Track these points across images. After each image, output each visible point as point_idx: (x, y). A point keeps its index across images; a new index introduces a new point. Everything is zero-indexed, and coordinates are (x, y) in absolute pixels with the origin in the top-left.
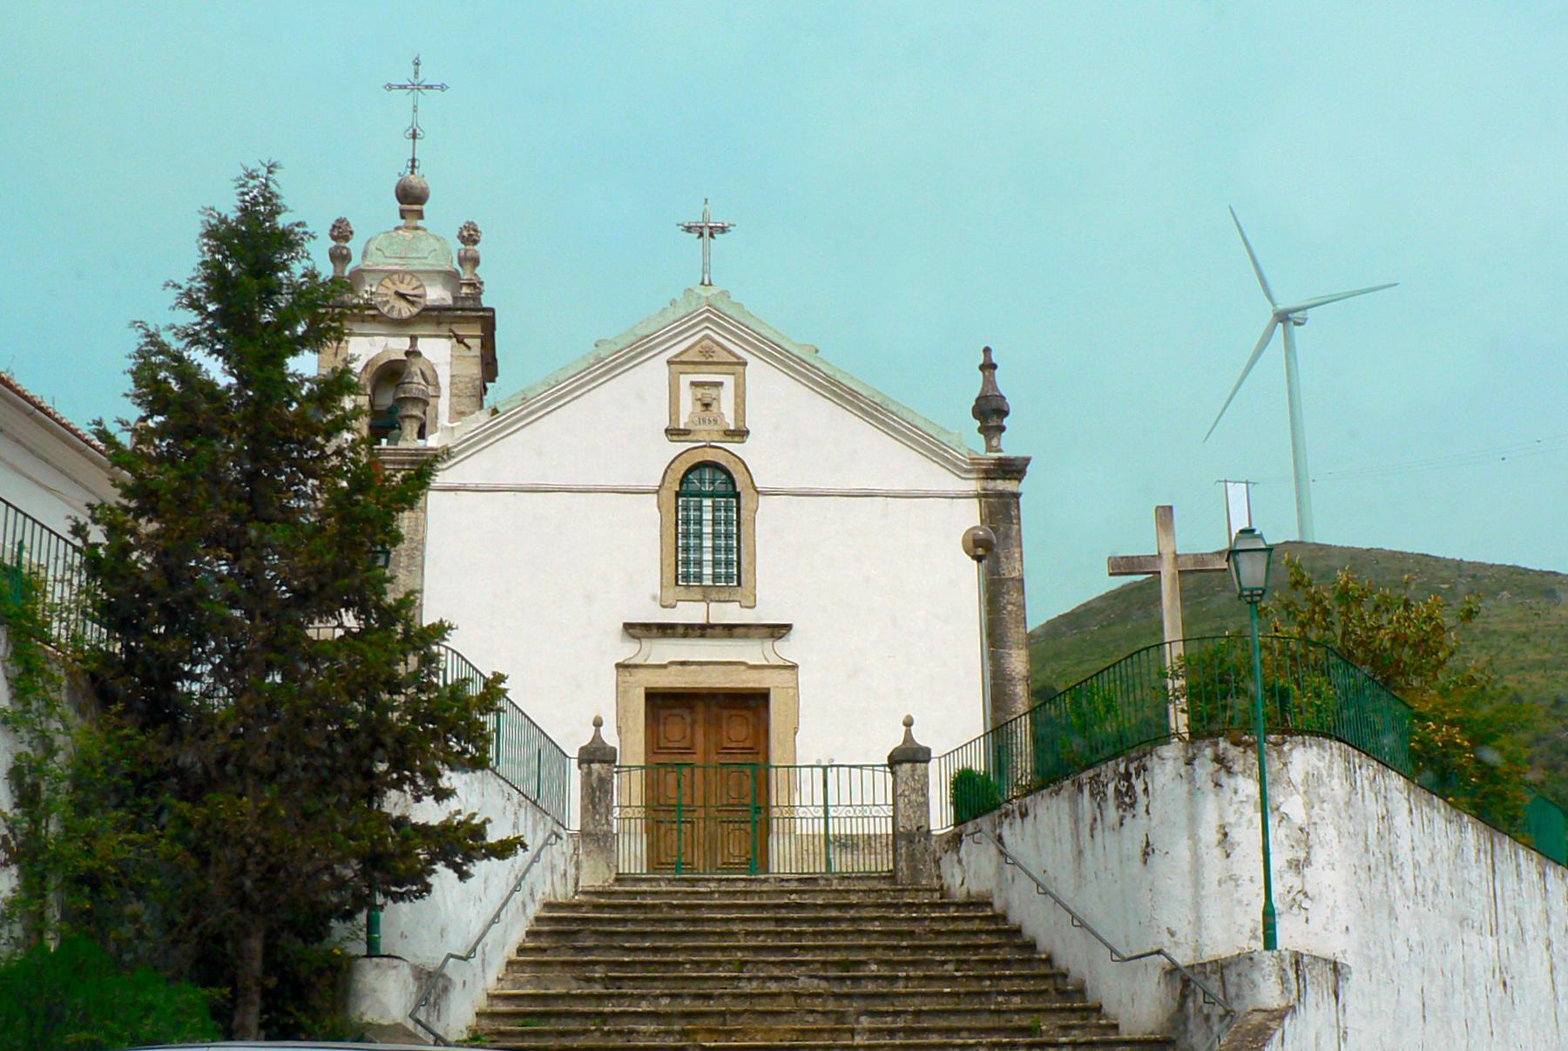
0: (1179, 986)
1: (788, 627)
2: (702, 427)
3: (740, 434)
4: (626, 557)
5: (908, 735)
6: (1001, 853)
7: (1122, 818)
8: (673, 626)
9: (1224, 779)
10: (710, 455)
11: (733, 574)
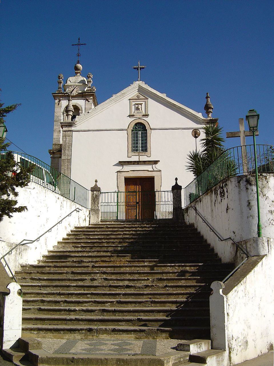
0: (235, 248)
1: (159, 161)
2: (138, 114)
3: (147, 115)
4: (120, 146)
5: (176, 182)
6: (196, 213)
7: (222, 200)
8: (131, 162)
9: (249, 186)
10: (140, 121)
11: (145, 149)
